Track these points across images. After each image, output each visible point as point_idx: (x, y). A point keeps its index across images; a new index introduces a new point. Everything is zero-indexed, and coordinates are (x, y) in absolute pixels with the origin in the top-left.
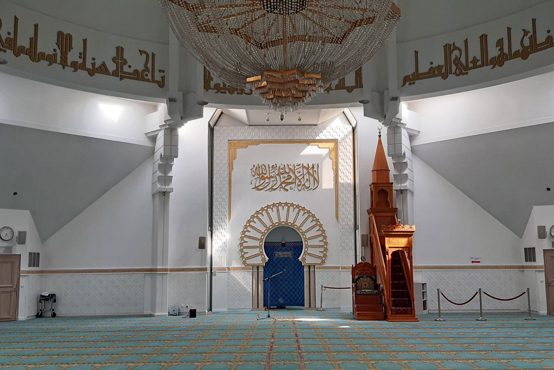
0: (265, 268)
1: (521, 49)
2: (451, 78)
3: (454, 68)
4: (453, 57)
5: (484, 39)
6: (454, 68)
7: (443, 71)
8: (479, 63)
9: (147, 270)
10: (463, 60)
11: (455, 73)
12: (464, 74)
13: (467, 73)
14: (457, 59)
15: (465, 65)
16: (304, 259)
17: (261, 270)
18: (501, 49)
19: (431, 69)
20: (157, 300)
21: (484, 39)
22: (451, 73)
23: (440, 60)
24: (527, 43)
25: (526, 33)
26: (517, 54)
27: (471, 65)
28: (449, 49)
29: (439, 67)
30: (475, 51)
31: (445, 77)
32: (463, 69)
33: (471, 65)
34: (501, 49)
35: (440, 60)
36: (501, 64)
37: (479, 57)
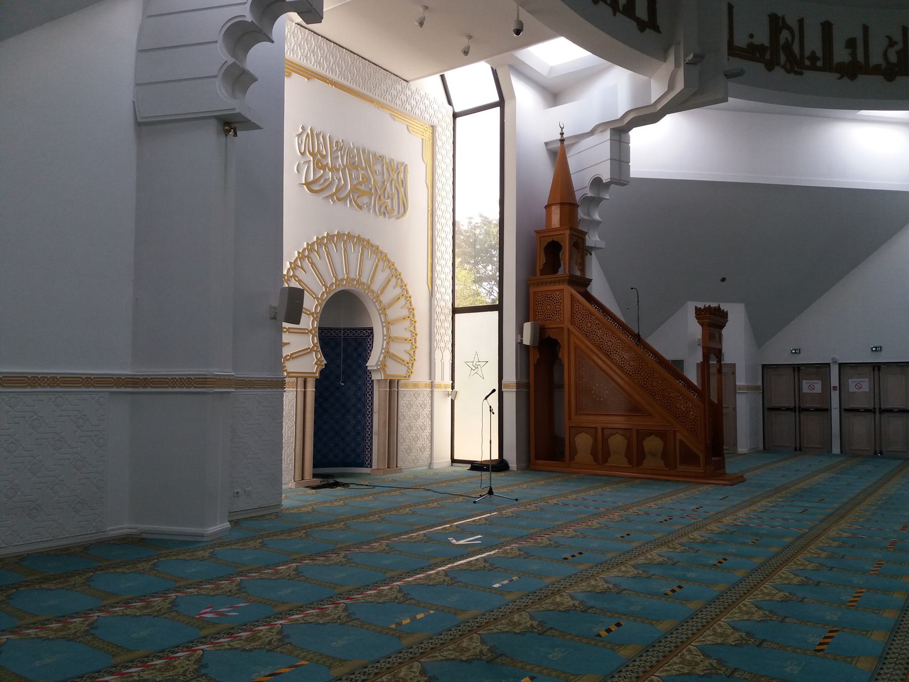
0: (318, 383)
1: (884, 65)
2: (779, 72)
3: (783, 58)
4: (782, 41)
5: (827, 27)
6: (783, 58)
7: (768, 56)
8: (819, 64)
9: (118, 381)
10: (796, 48)
11: (784, 67)
12: (796, 73)
13: (801, 74)
14: (788, 47)
15: (798, 56)
16: (383, 366)
17: (311, 389)
18: (854, 54)
19: (750, 45)
20: (284, 466)
21: (827, 27)
22: (778, 64)
23: (762, 38)
24: (893, 58)
25: (892, 43)
26: (876, 70)
27: (807, 63)
28: (776, 23)
29: (761, 48)
30: (813, 43)
31: (770, 66)
32: (797, 65)
33: (807, 63)
34: (854, 54)
35: (762, 38)
36: (853, 77)
37: (819, 54)
